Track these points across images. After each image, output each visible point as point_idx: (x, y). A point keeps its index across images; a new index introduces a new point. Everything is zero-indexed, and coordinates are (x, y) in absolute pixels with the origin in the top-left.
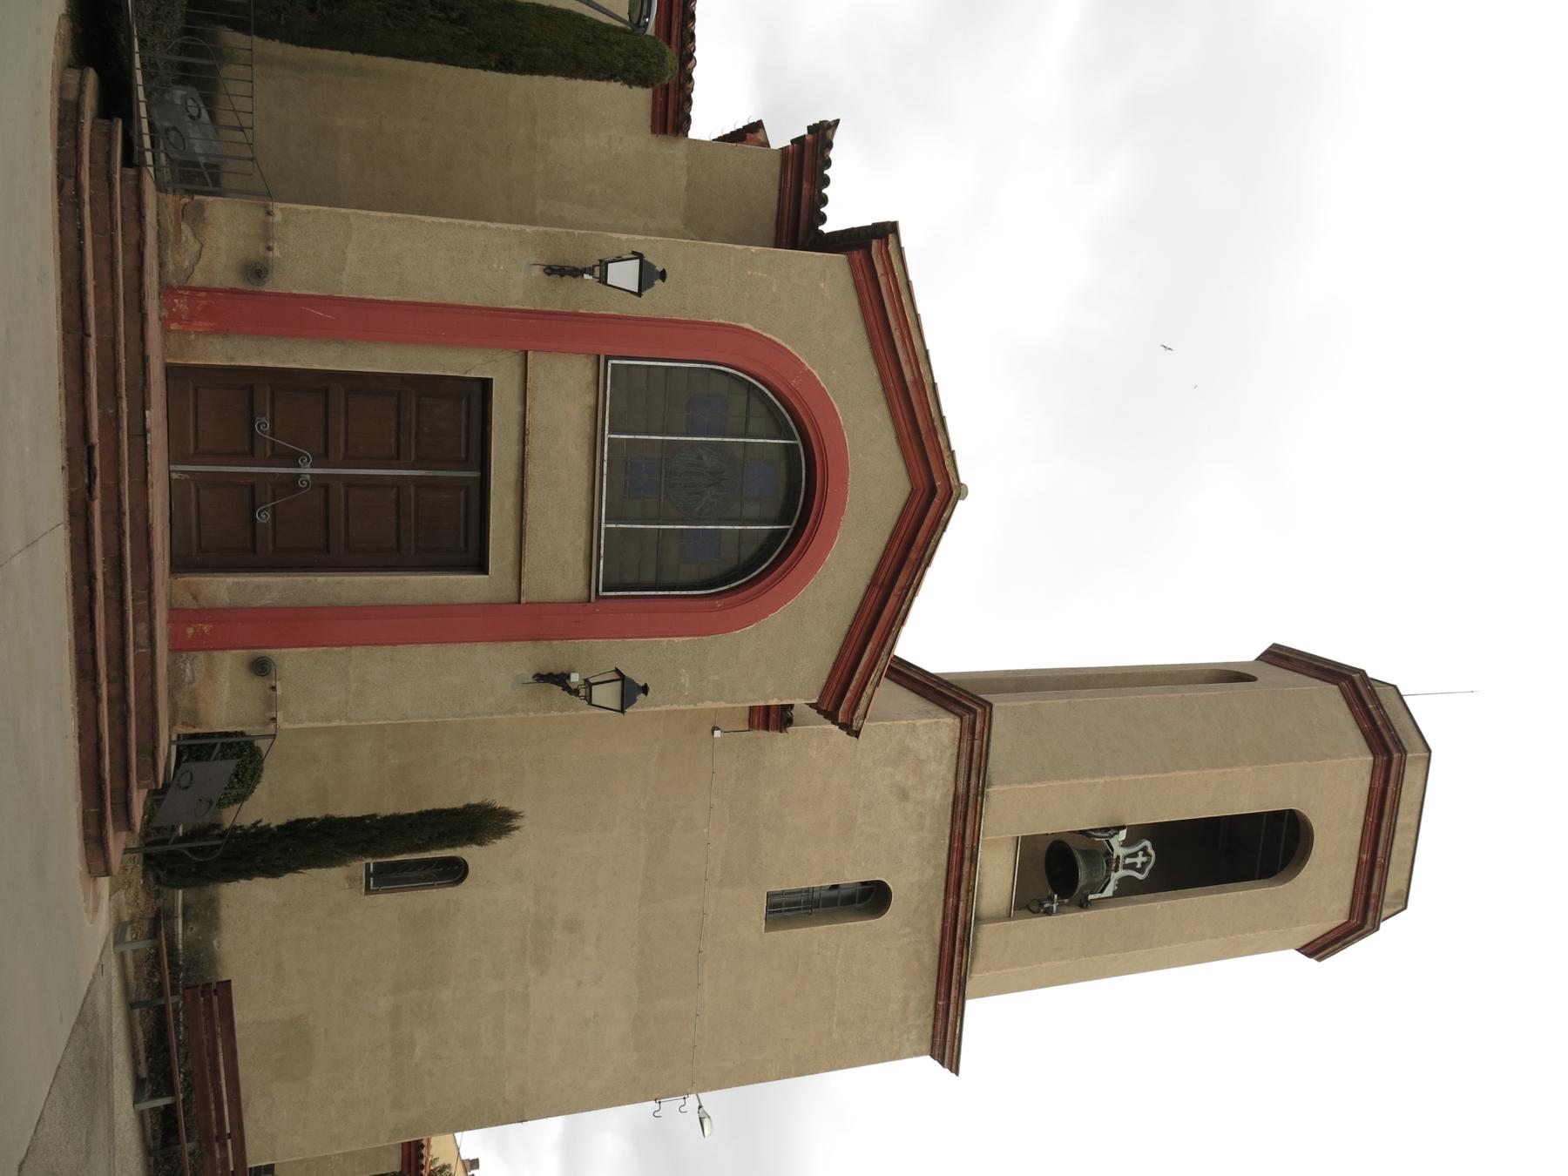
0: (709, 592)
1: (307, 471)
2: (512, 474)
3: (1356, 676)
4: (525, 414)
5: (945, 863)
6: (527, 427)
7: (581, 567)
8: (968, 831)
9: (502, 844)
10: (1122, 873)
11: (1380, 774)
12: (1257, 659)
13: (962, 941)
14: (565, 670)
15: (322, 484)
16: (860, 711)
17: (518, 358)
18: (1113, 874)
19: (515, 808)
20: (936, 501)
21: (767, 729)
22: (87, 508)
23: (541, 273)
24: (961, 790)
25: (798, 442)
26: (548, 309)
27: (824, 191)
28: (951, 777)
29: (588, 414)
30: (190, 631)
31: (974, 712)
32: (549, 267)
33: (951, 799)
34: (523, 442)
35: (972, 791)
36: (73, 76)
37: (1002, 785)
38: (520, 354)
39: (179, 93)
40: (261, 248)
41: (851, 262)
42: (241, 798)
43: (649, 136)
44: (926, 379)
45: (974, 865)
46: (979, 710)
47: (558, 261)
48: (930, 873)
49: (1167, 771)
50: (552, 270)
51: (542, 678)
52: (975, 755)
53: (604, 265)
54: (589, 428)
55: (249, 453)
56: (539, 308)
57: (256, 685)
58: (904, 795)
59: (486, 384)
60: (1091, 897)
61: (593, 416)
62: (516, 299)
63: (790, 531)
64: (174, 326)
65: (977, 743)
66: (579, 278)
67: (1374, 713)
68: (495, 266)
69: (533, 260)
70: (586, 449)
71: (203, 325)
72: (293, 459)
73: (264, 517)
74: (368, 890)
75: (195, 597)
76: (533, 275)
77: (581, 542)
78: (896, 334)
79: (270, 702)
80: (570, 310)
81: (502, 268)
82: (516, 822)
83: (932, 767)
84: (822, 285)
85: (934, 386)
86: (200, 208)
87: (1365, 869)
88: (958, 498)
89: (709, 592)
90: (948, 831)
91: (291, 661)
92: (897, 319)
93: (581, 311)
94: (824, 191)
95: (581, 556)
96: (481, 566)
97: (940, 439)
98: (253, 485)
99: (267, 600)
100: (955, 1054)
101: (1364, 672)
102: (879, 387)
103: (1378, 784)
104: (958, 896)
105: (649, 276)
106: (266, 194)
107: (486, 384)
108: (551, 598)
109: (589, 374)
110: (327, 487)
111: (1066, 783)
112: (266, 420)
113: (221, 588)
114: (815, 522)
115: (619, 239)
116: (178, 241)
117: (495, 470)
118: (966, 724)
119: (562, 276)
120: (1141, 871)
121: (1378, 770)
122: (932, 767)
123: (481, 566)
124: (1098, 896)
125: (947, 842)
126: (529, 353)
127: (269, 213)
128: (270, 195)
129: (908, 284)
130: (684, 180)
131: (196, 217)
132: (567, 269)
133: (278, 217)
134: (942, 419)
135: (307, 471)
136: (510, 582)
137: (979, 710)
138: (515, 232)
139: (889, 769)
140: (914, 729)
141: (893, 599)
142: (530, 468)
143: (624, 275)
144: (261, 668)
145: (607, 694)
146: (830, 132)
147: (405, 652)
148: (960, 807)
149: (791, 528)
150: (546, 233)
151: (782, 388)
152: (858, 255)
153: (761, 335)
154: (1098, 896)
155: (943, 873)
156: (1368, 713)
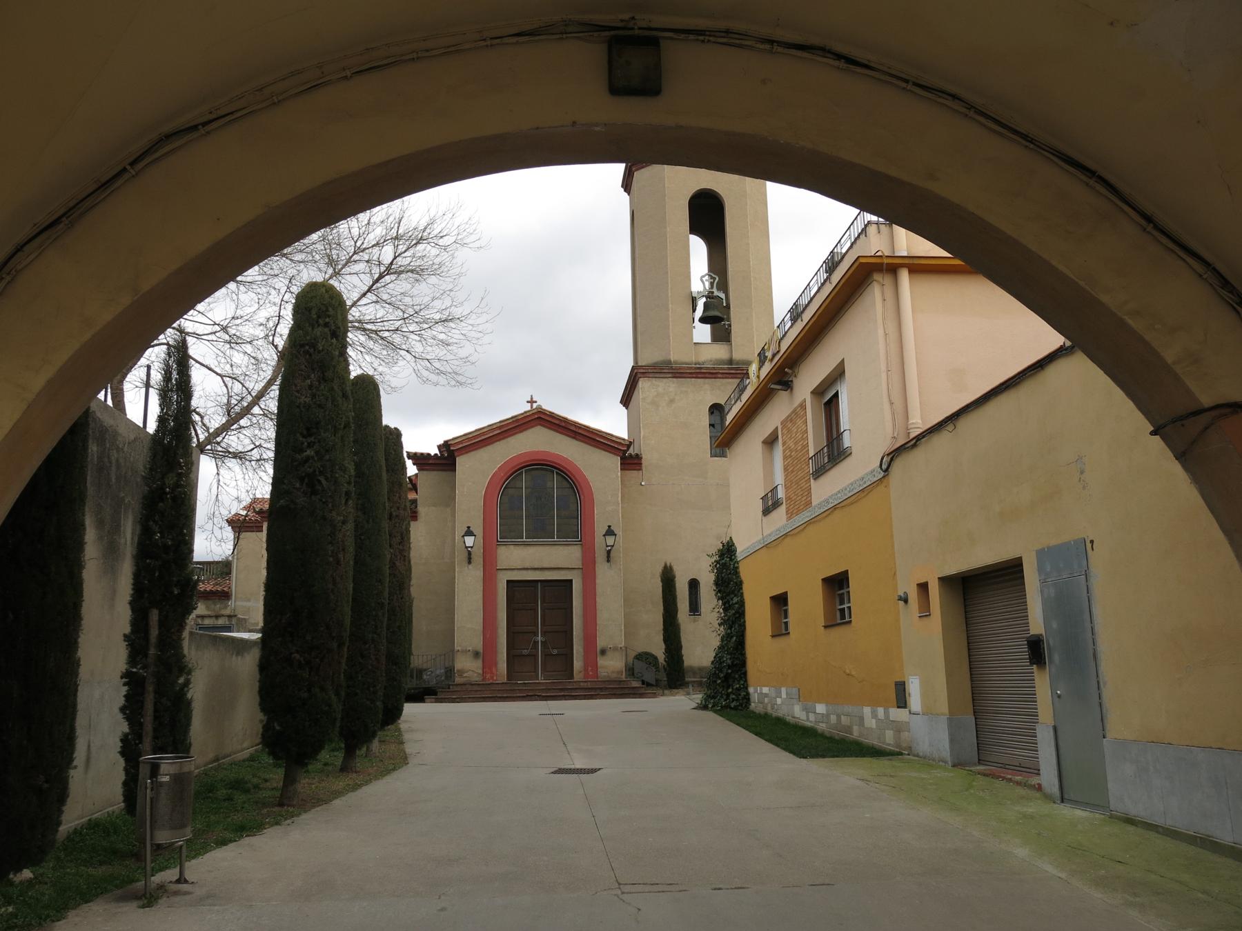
1: (540, 638)
2: (538, 572)
5: (702, 380)
7: (570, 548)
8: (688, 371)
9: (675, 568)
10: (715, 290)
12: (629, 195)
13: (737, 370)
15: (544, 633)
16: (622, 442)
17: (499, 572)
18: (715, 294)
19: (663, 565)
20: (543, 416)
21: (641, 464)
22: (544, 696)
24: (670, 375)
25: (524, 470)
26: (482, 563)
27: (432, 455)
28: (665, 380)
29: (517, 547)
30: (591, 673)
31: (636, 373)
33: (674, 379)
34: (527, 569)
35: (671, 371)
36: (426, 700)
37: (670, 354)
39: (425, 677)
40: (468, 653)
41: (459, 456)
42: (656, 658)
43: (418, 522)
44: (499, 425)
46: (635, 371)
48: (707, 387)
49: (667, 272)
50: (470, 562)
51: (608, 559)
52: (655, 371)
53: (467, 547)
54: (522, 547)
55: (535, 656)
57: (609, 654)
58: (672, 401)
59: (508, 582)
60: (725, 305)
62: (480, 573)
64: (495, 678)
65: (649, 371)
70: (528, 548)
71: (494, 670)
72: (536, 643)
73: (555, 652)
74: (700, 615)
75: (580, 672)
77: (561, 548)
78: (483, 438)
79: (615, 649)
80: (482, 555)
82: (668, 565)
83: (660, 389)
84: (467, 466)
85: (500, 422)
86: (458, 671)
90: (689, 379)
91: (601, 643)
92: (478, 438)
94: (432, 455)
95: (566, 547)
96: (571, 581)
98: (545, 655)
99: (581, 650)
105: (469, 533)
106: (451, 653)
107: (508, 582)
108: (581, 558)
109: (503, 547)
110: (545, 632)
111: (671, 324)
112: (523, 651)
113: (578, 664)
116: (469, 677)
118: (642, 376)
120: (714, 279)
122: (660, 389)
123: (571, 581)
124: (724, 301)
125: (693, 379)
127: (458, 651)
128: (453, 651)
129: (465, 435)
130: (434, 508)
131: (461, 672)
133: (459, 648)
134: (512, 418)
135: (540, 638)
136: (575, 571)
137: (635, 371)
139: (660, 409)
140: (644, 399)
141: (580, 431)
142: (536, 566)
143: (469, 541)
144: (603, 652)
145: (610, 540)
146: (411, 454)
147: (599, 607)
148: (678, 375)
149: (555, 470)
151: (505, 478)
154: (724, 301)
155: (707, 380)
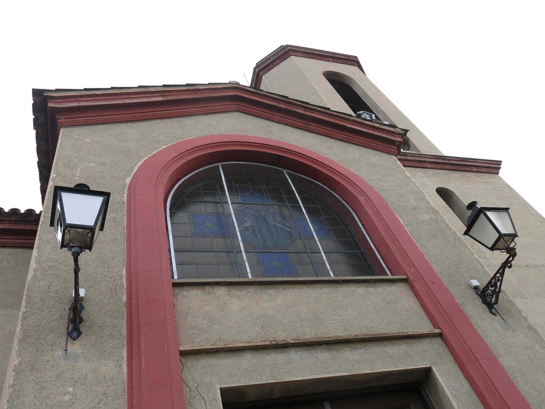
0: (352, 211)
3: (257, 70)
4: (297, 252)
6: (268, 343)
11: (297, 54)
14: (473, 292)
23: (77, 343)
26: (124, 332)
32: (69, 334)
38: (183, 361)
45: (408, 154)
47: (63, 325)
56: (125, 342)
61: (237, 287)
63: (286, 171)
66: (84, 304)
67: (272, 60)
68: (67, 398)
69: (60, 353)
76: (80, 351)
80: (124, 309)
81: (71, 389)
87: (335, 60)
88: (239, 84)
89: (352, 211)
93: (125, 299)
97: (202, 88)
100: (493, 162)
101: (254, 68)
102: (167, 121)
103: (302, 55)
104: (424, 162)
109: (195, 294)
114: (278, 150)
115: (35, 270)
117: (325, 373)
119: (81, 320)
121: (296, 54)
126: (182, 348)
132: (71, 317)
138: (16, 378)
150: (22, 341)
152: (61, 119)
153: (136, 173)
156: (272, 62)
